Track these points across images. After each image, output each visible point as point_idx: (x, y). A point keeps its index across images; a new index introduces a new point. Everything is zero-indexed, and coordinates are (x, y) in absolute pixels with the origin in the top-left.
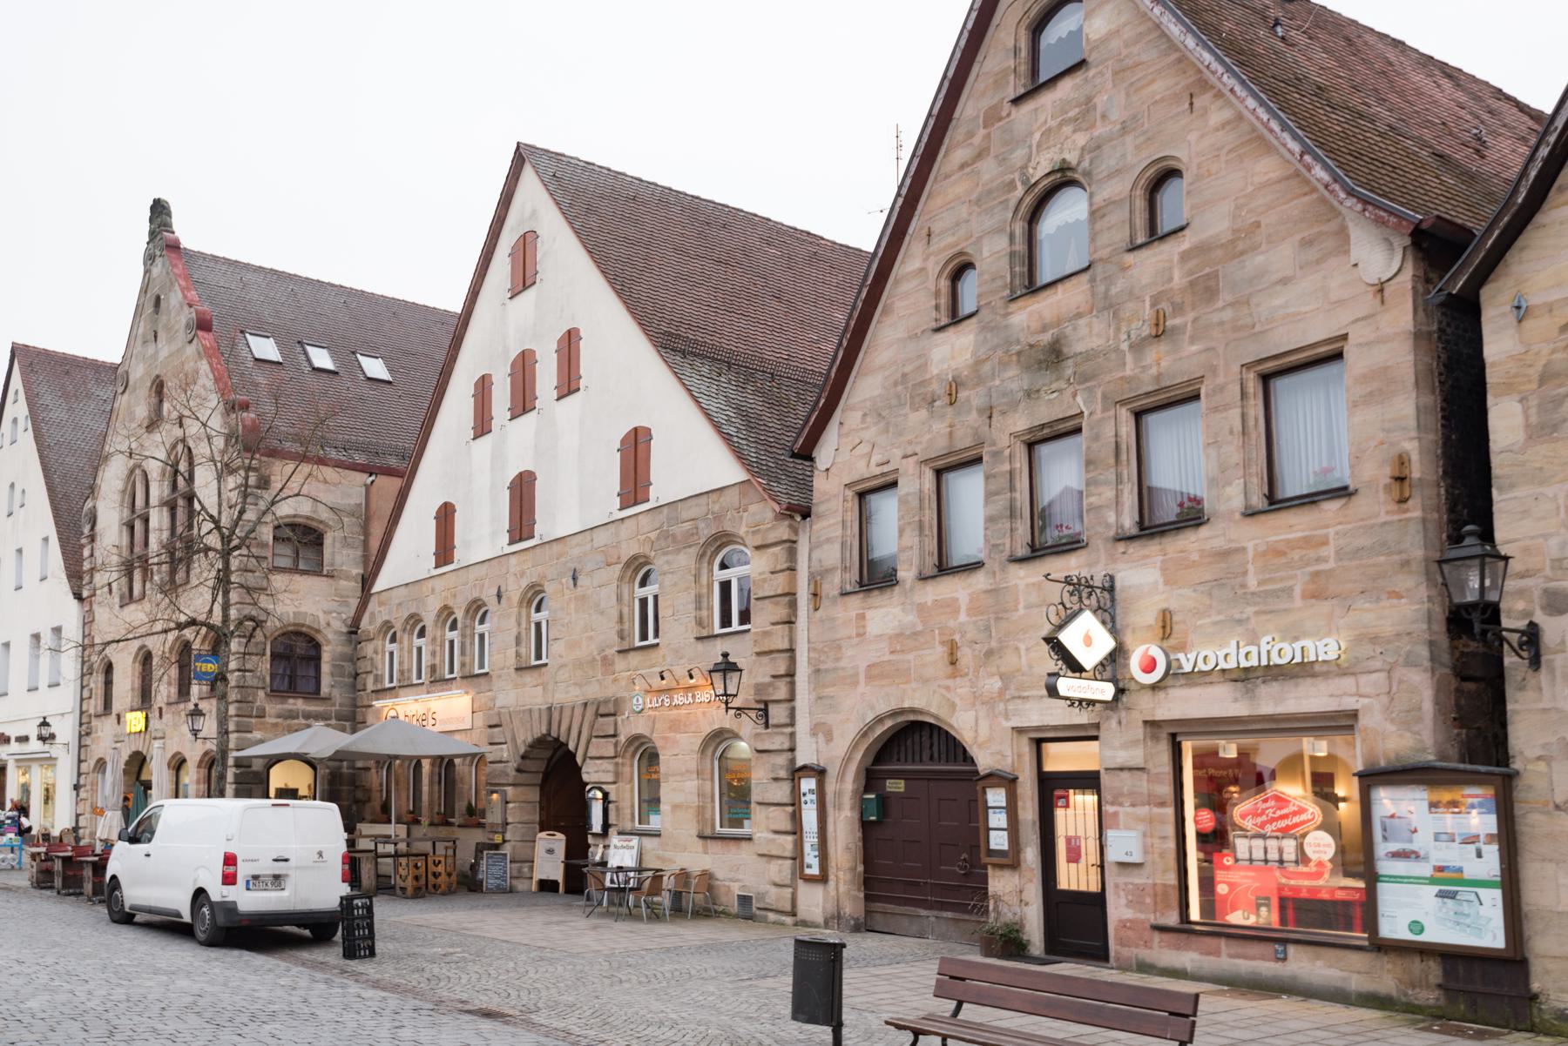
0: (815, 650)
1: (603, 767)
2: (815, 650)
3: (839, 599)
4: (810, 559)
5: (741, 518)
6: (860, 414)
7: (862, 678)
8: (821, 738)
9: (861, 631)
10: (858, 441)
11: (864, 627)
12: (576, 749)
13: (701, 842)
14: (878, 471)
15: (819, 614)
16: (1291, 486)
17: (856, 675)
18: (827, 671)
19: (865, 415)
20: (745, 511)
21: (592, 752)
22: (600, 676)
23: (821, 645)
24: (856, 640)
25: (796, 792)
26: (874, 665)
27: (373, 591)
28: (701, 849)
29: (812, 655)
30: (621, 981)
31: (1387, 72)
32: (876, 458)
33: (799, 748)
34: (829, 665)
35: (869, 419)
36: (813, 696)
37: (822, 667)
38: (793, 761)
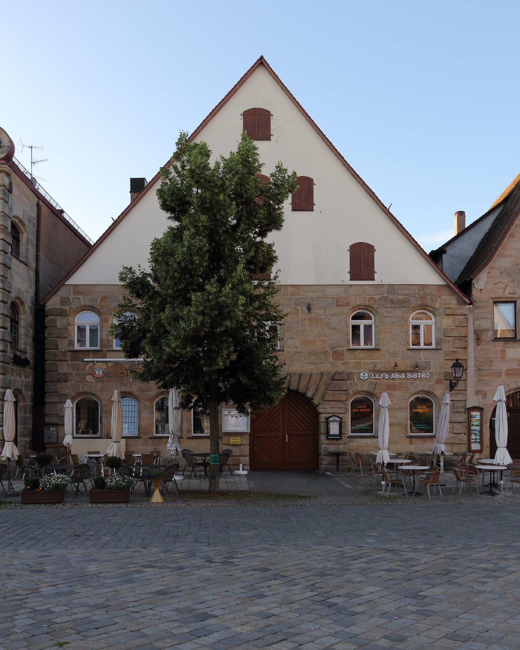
0: (478, 361)
1: (337, 406)
2: (478, 361)
3: (491, 342)
4: (474, 324)
5: (437, 300)
6: (499, 272)
7: (503, 374)
8: (480, 396)
9: (503, 356)
10: (497, 282)
11: (505, 355)
12: (314, 395)
13: (408, 439)
14: (510, 296)
15: (479, 347)
16: (513, 336)
17: (501, 372)
18: (484, 370)
19: (501, 273)
20: (439, 297)
21: (327, 397)
22: (331, 360)
23: (481, 359)
24: (500, 359)
25: (470, 417)
26: (510, 370)
27: (67, 283)
28: (408, 443)
29: (476, 363)
30: (397, 505)
31: (459, 224)
32: (507, 291)
33: (468, 400)
34: (486, 367)
35: (504, 275)
36: (477, 379)
37: (481, 368)
38: (465, 405)
